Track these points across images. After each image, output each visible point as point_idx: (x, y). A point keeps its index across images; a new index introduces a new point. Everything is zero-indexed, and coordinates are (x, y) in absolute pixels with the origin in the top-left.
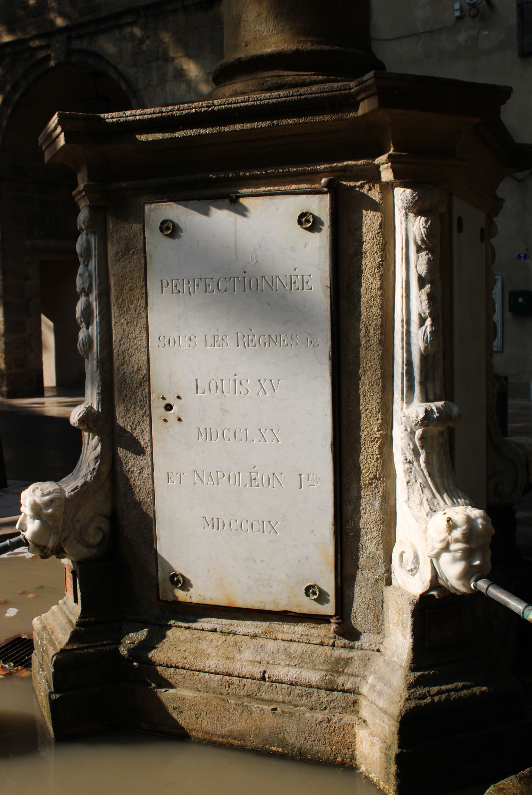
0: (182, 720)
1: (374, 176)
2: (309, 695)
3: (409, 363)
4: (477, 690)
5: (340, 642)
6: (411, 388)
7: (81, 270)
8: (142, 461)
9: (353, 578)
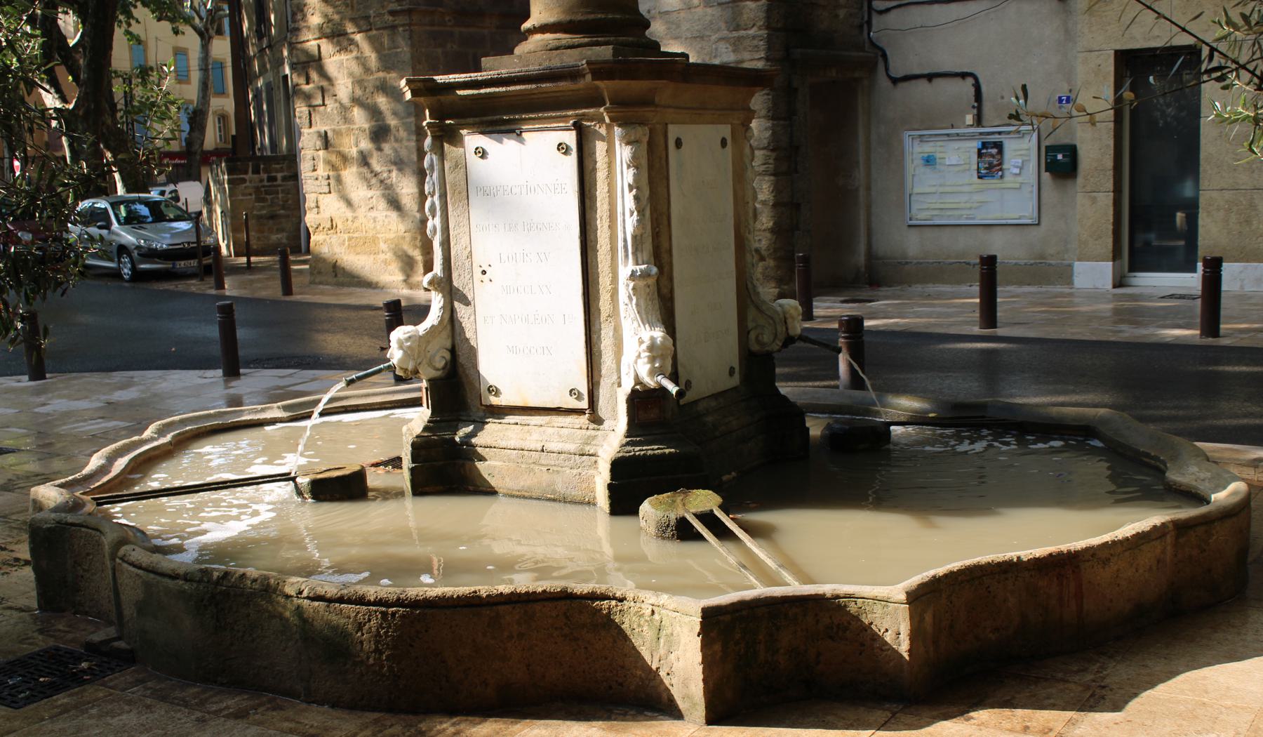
0: (493, 482)
1: (601, 121)
2: (569, 460)
3: (625, 240)
4: (667, 451)
5: (592, 426)
6: (627, 256)
7: (428, 179)
8: (469, 310)
9: (599, 383)
